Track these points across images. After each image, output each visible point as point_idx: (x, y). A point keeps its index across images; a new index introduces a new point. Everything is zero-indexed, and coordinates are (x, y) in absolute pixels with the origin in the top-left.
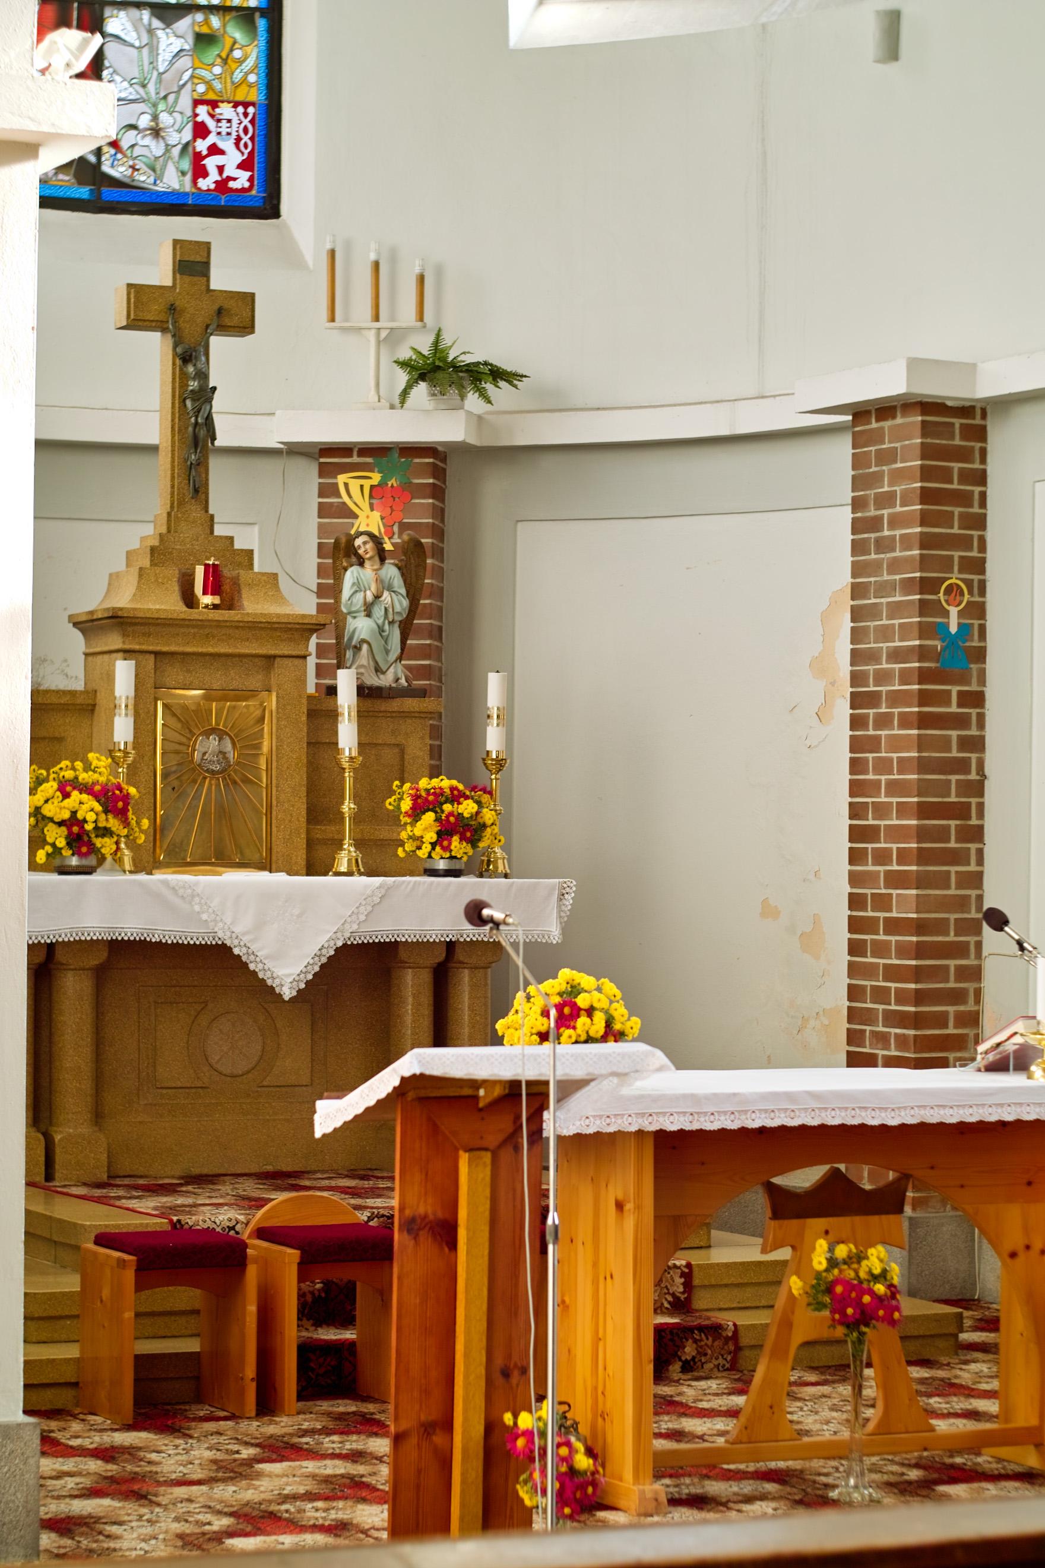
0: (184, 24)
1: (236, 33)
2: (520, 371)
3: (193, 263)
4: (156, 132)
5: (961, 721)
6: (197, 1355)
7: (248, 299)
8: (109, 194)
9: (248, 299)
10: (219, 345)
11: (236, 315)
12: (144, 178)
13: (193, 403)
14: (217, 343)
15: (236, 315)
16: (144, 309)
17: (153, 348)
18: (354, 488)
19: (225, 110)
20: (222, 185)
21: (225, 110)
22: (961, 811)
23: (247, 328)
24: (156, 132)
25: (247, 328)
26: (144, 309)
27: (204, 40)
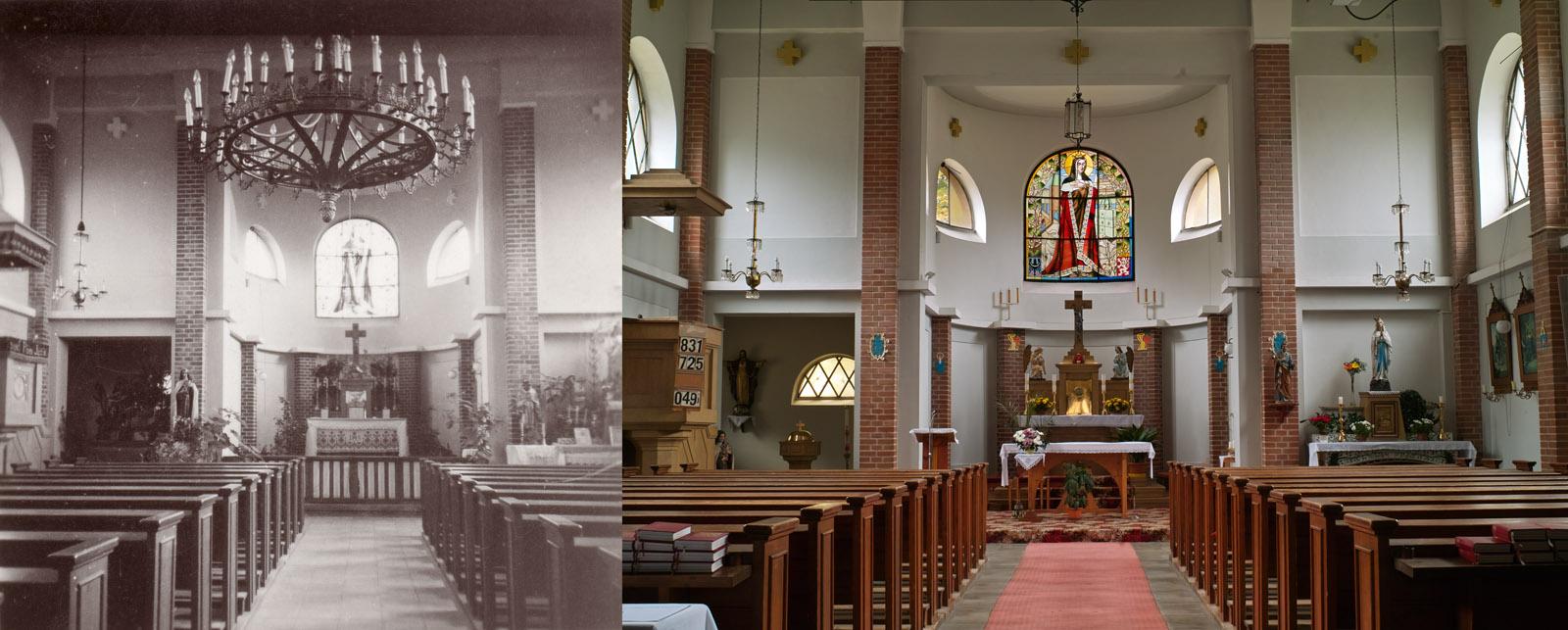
0: (1115, 242)
1: (1125, 242)
2: (253, 340)
3: (1078, 295)
4: (1109, 265)
5: (1222, 380)
6: (1299, 599)
7: (1090, 302)
8: (1101, 278)
9: (1090, 302)
10: (361, 339)
11: (1088, 305)
12: (1107, 275)
13: (1079, 320)
14: (1084, 311)
15: (1088, 305)
16: (1069, 305)
17: (350, 339)
18: (1140, 337)
19: (1124, 259)
20: (1123, 274)
21: (1124, 259)
22: (1223, 399)
23: (365, 336)
24: (1109, 265)
25: (365, 336)
26: (1069, 305)
27: (1119, 245)
